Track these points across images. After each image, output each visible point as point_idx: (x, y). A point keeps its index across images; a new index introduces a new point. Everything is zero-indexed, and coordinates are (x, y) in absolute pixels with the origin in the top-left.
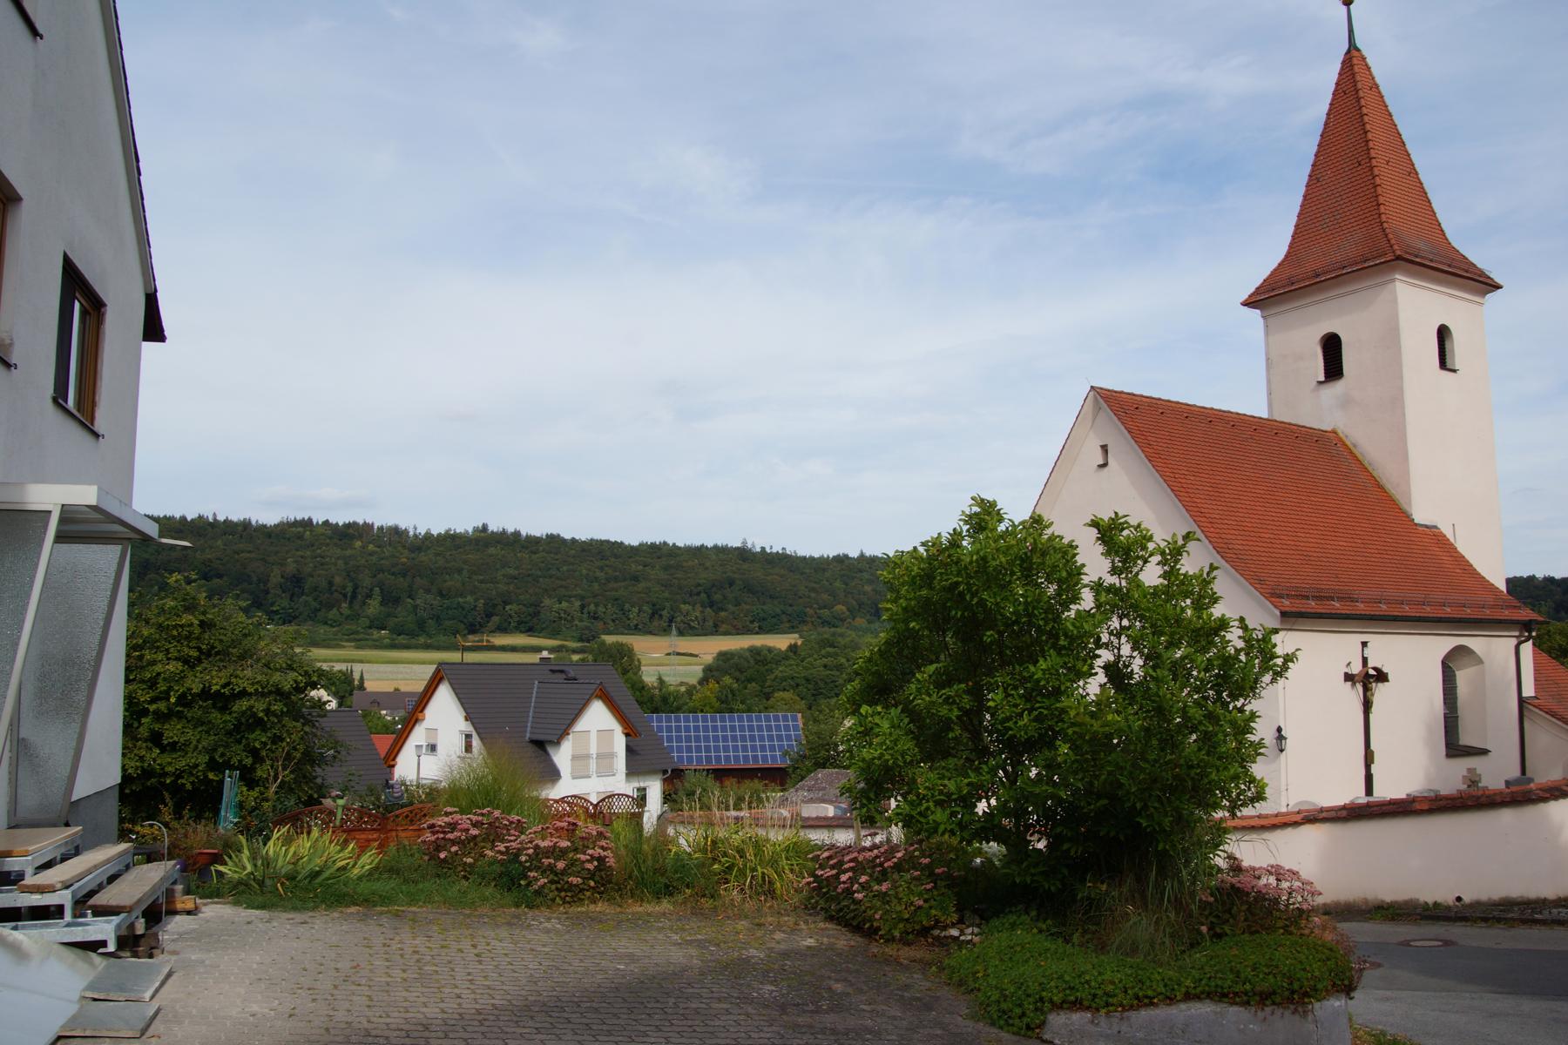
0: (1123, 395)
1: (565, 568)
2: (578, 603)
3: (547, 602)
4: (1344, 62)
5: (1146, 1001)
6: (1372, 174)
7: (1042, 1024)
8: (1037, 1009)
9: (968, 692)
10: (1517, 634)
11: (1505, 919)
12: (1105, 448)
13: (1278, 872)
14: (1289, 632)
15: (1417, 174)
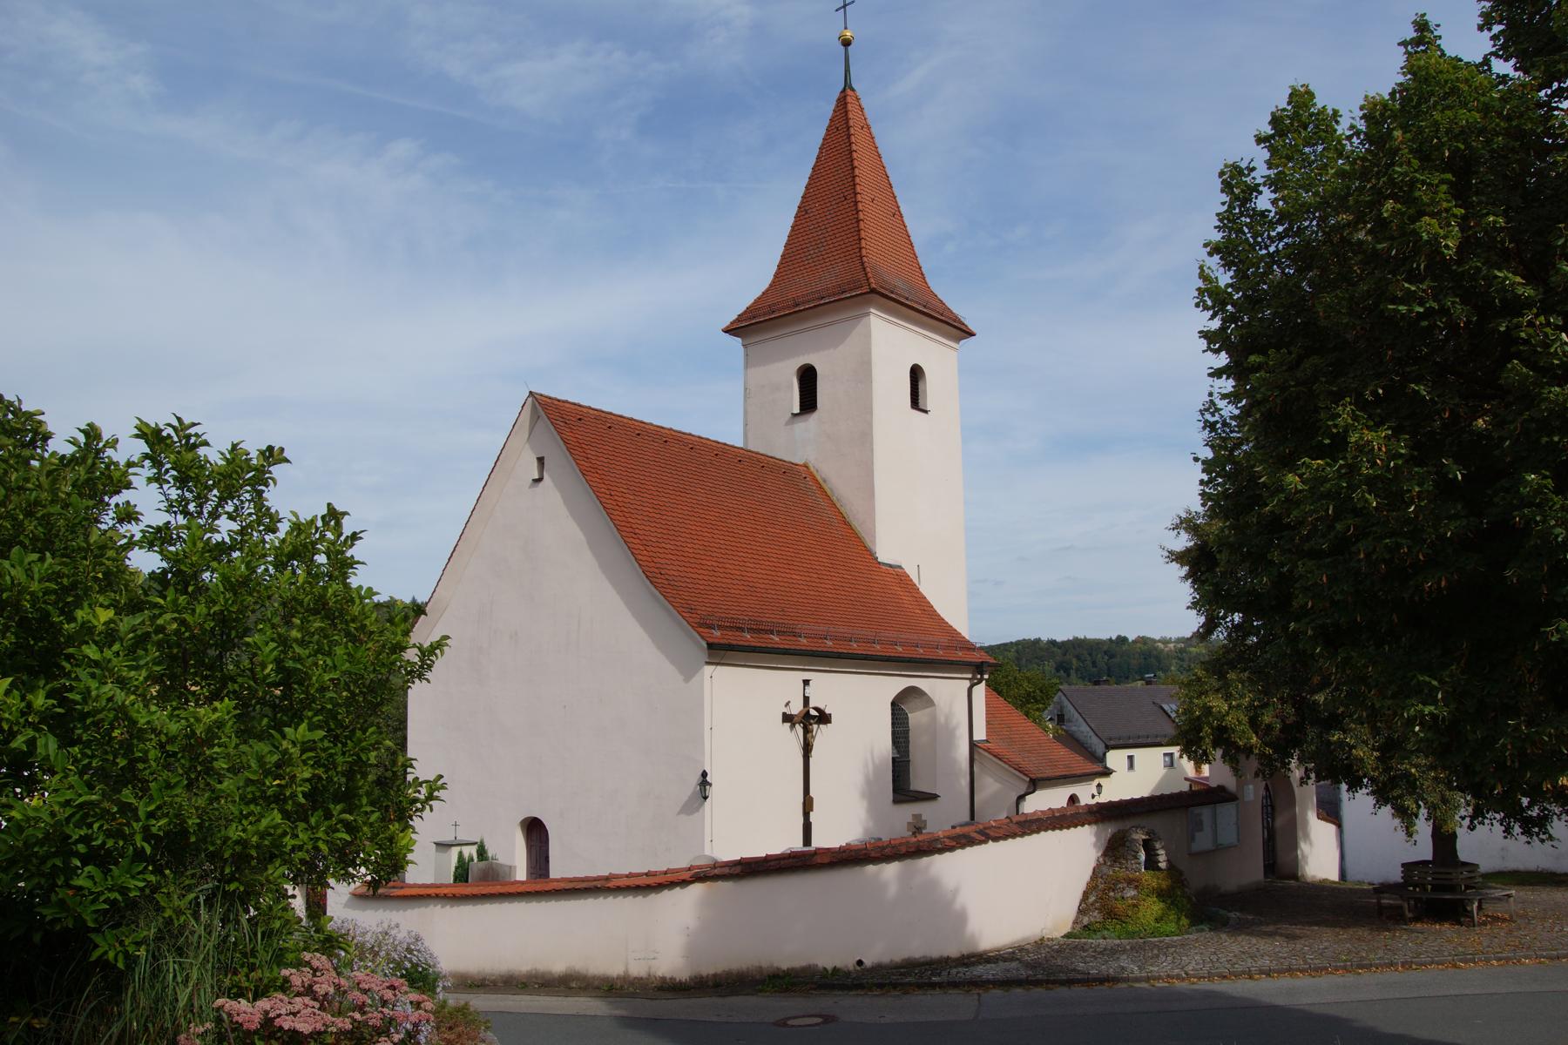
0: (567, 405)
10: (970, 676)
11: (902, 984)
12: (541, 460)
14: (719, 667)
15: (901, 216)
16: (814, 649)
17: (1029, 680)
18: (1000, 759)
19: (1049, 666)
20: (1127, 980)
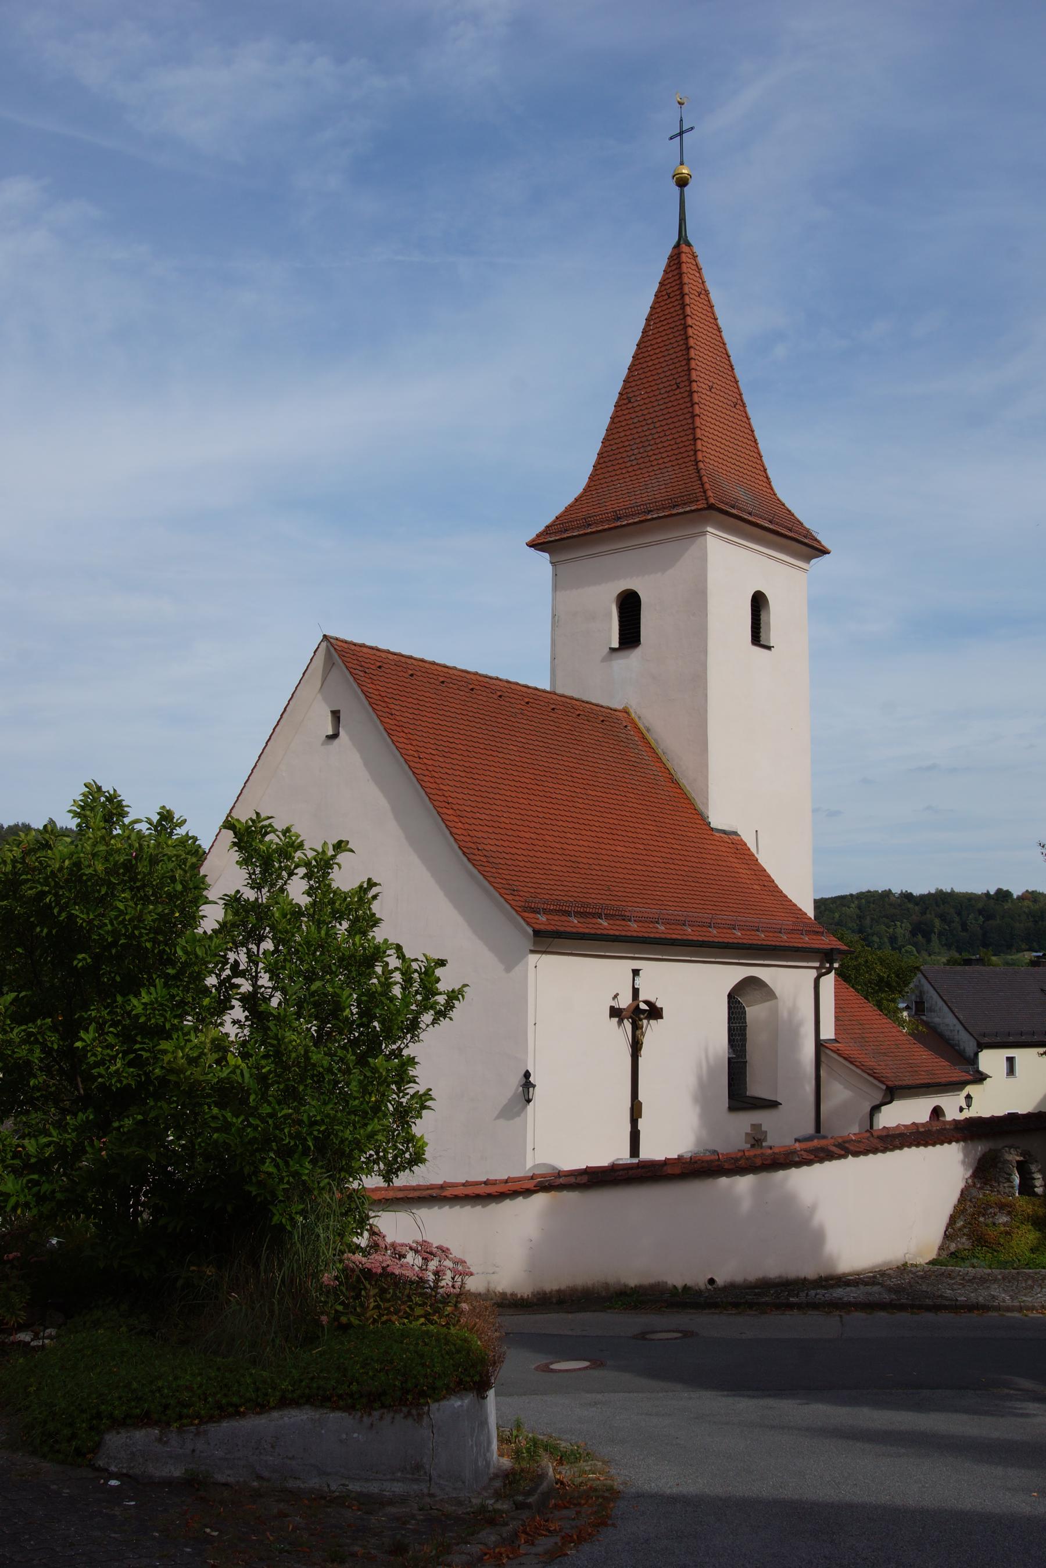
0: (365, 650)
4: (671, 258)
5: (231, 1410)
6: (691, 400)
7: (98, 1445)
8: (91, 1428)
9: (54, 1028)
10: (817, 964)
12: (336, 715)
13: (426, 1251)
14: (544, 956)
15: (744, 406)
16: (646, 935)
17: (882, 961)
18: (851, 1062)
19: (902, 929)
20: (998, 1308)
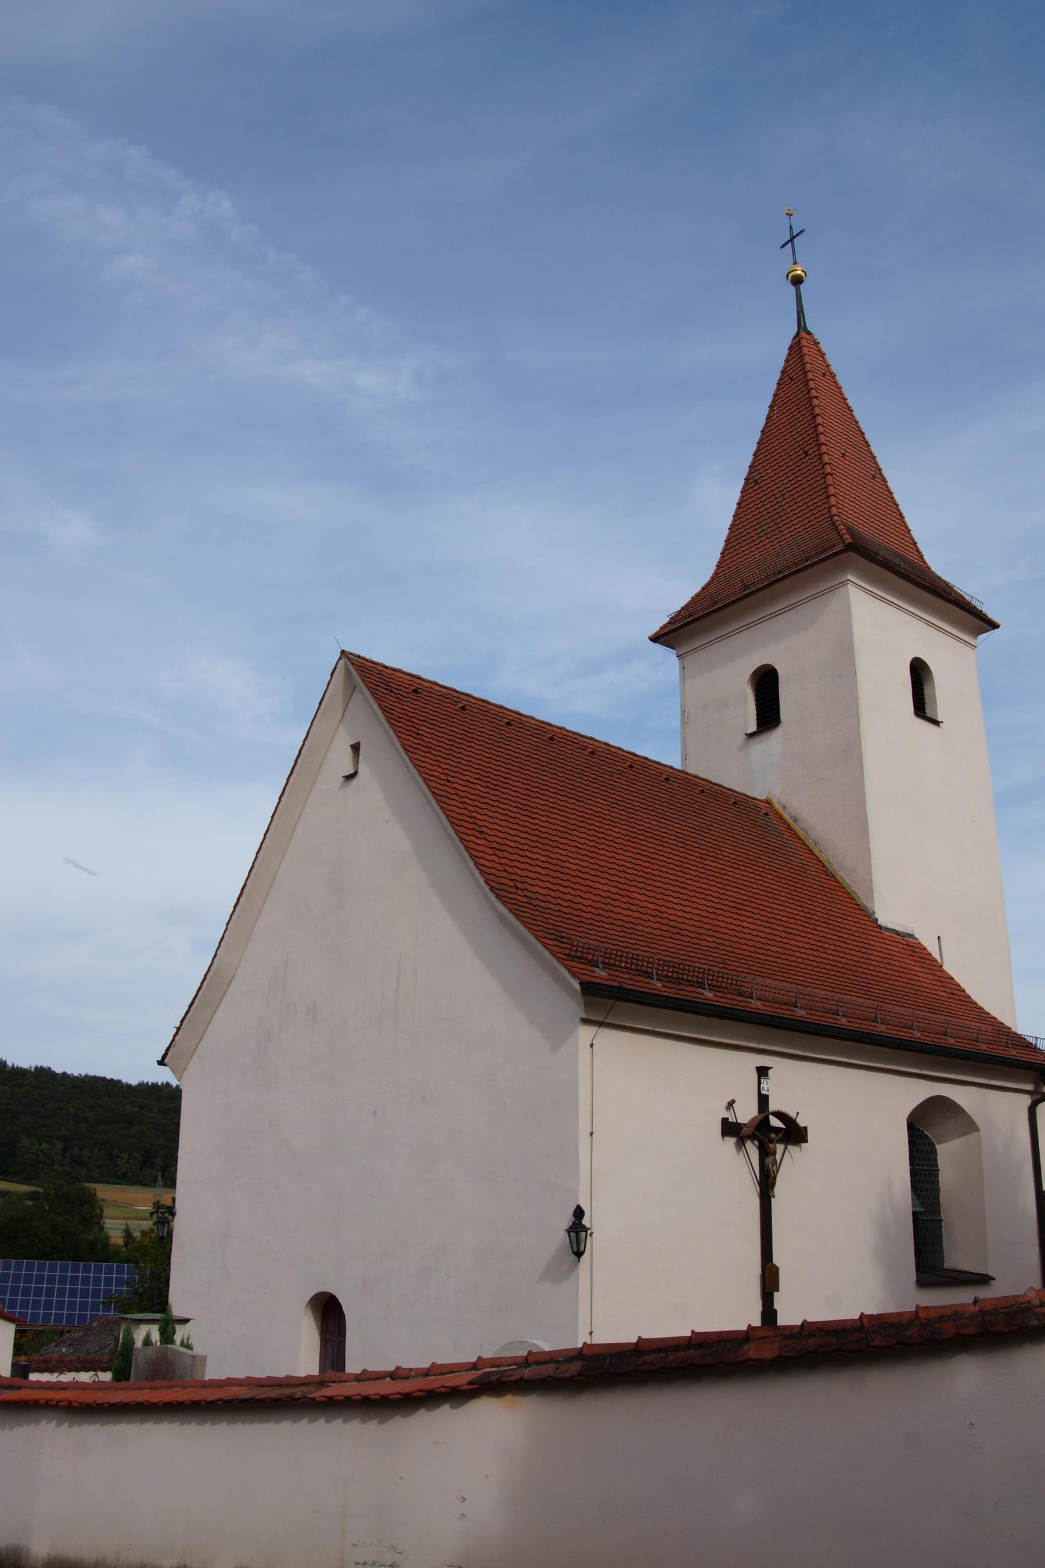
1: (51, 1105)
2: (60, 1146)
3: (25, 1142)
4: (791, 348)
10: (1030, 1087)
12: (356, 748)
